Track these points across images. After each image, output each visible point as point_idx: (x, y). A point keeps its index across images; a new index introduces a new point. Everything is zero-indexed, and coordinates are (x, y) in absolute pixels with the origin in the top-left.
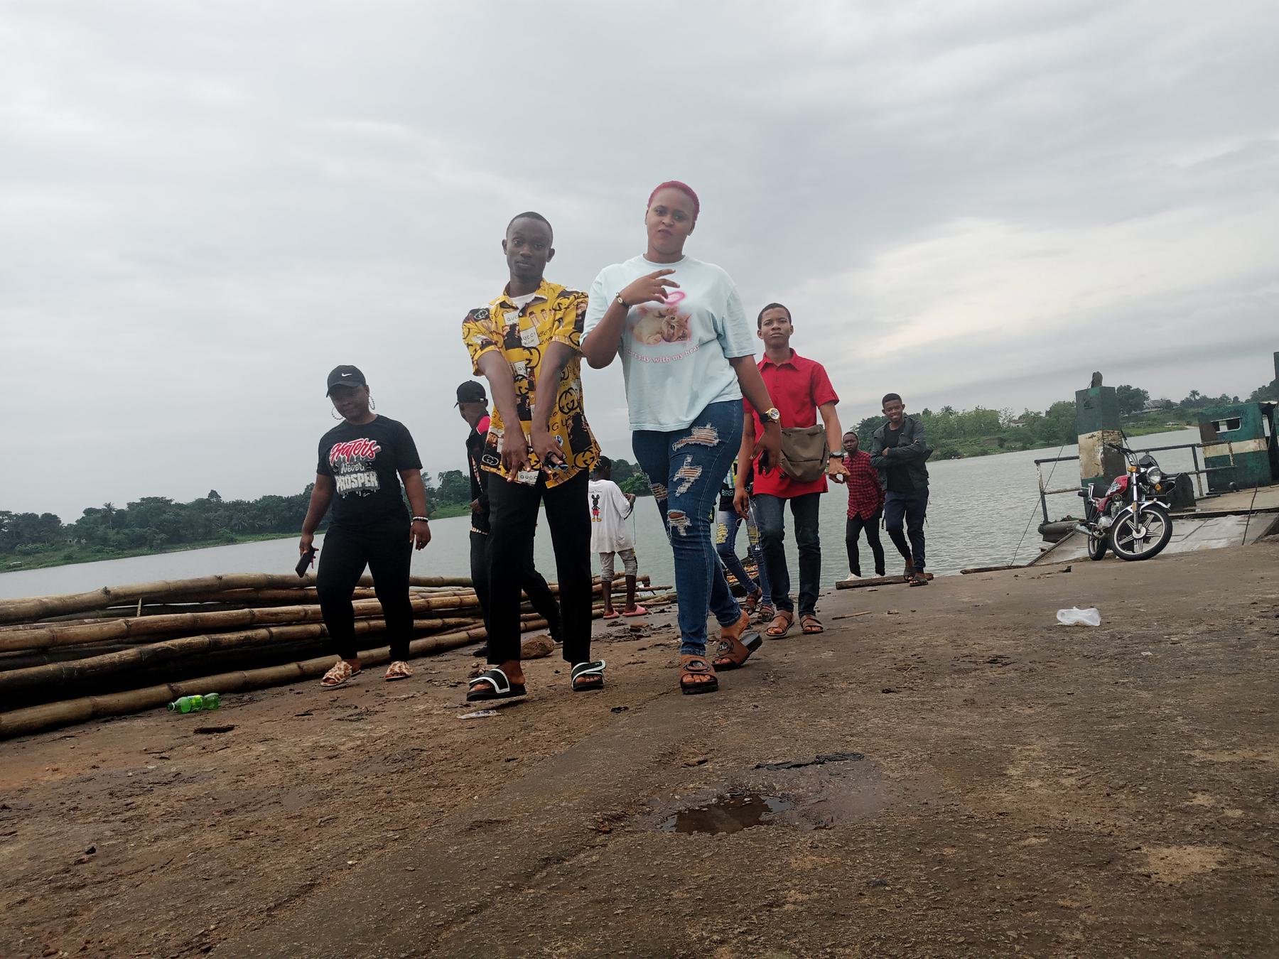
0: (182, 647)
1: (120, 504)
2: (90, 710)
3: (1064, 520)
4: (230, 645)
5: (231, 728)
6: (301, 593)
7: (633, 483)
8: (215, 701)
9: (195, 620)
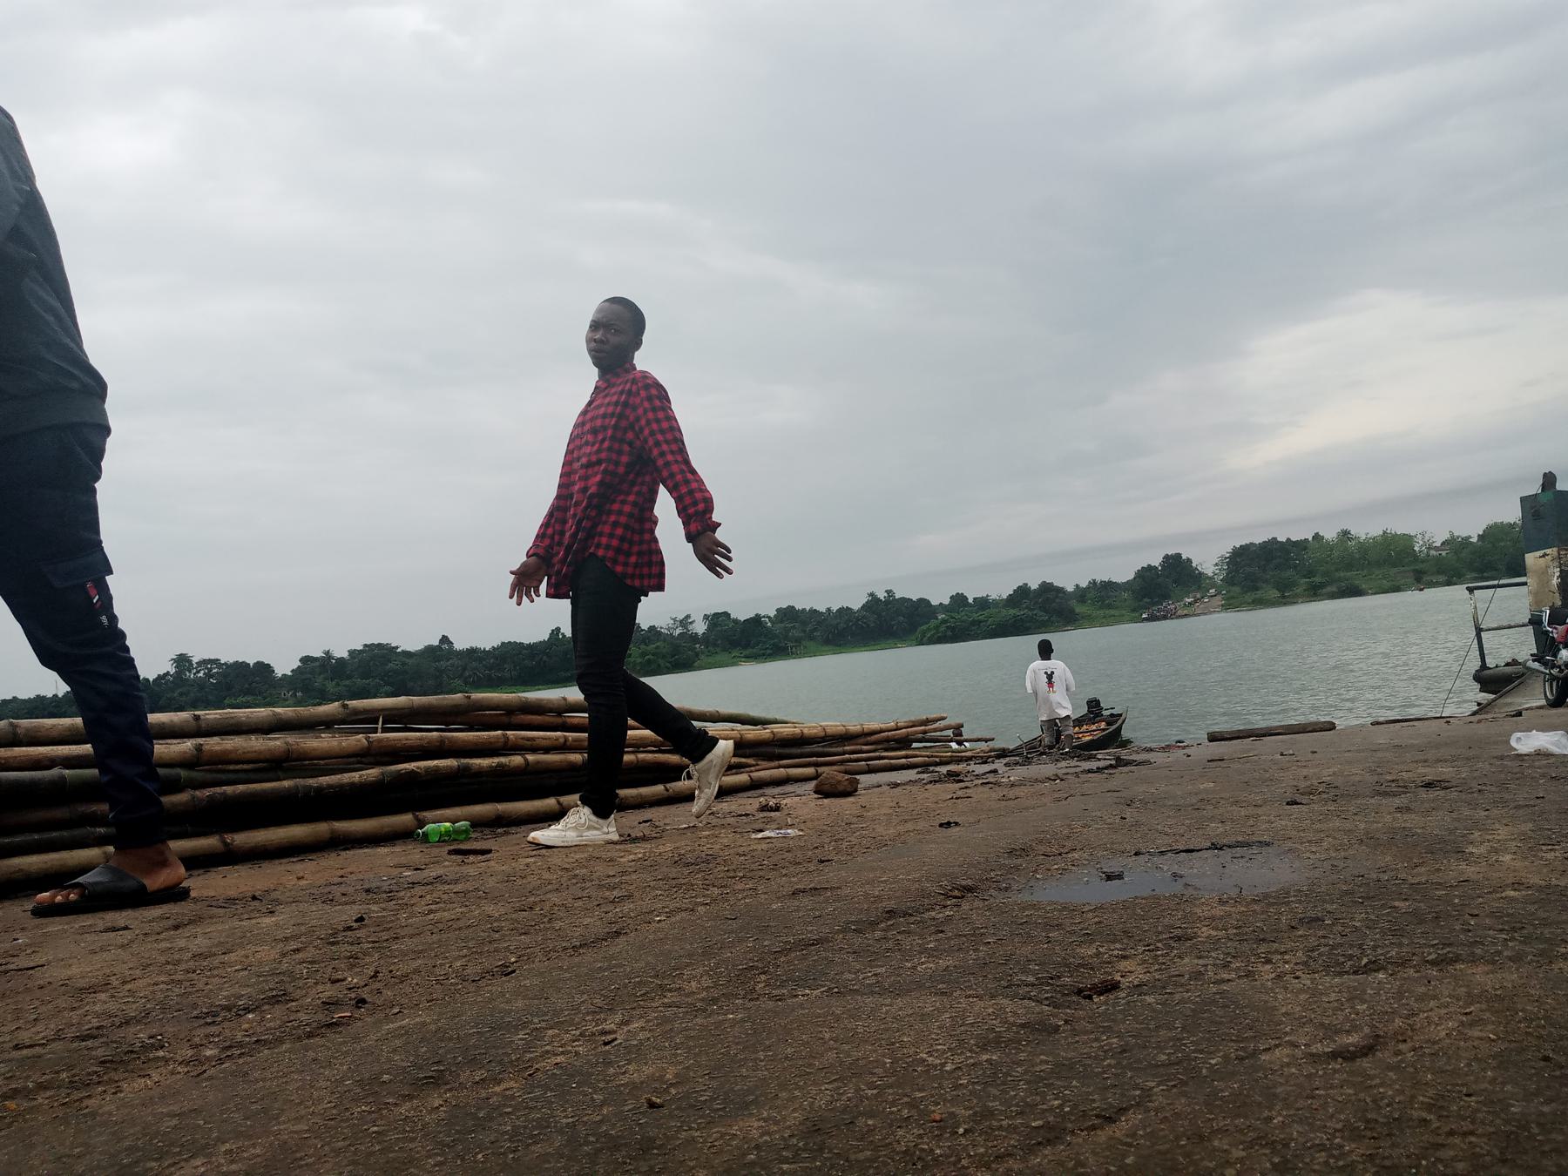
0: (427, 769)
1: (341, 652)
2: (328, 836)
3: (1507, 664)
4: (480, 773)
5: (489, 851)
6: (559, 720)
7: (937, 628)
8: (466, 831)
9: (442, 741)
